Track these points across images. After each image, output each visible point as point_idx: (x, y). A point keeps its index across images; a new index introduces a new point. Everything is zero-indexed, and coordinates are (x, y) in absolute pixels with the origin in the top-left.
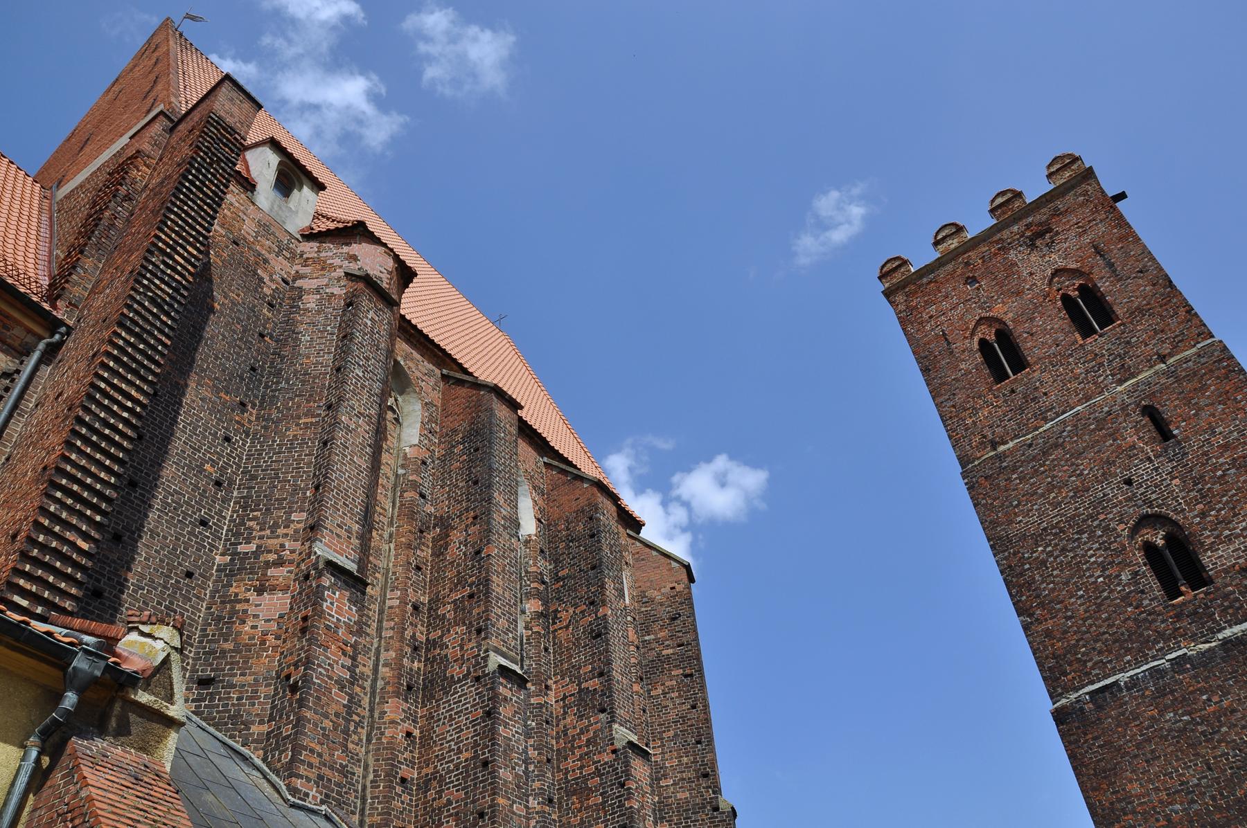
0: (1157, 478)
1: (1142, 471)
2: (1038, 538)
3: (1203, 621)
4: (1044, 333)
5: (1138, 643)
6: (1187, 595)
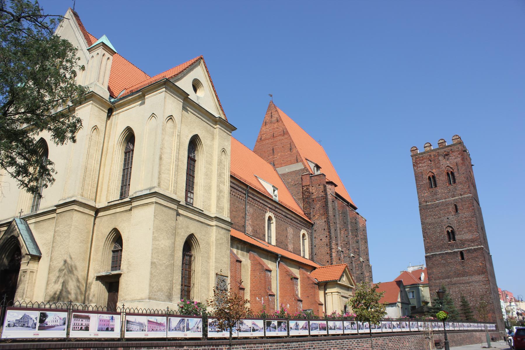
0: (452, 219)
1: (451, 217)
2: (430, 224)
3: (452, 246)
4: (442, 179)
5: (441, 248)
6: (452, 242)
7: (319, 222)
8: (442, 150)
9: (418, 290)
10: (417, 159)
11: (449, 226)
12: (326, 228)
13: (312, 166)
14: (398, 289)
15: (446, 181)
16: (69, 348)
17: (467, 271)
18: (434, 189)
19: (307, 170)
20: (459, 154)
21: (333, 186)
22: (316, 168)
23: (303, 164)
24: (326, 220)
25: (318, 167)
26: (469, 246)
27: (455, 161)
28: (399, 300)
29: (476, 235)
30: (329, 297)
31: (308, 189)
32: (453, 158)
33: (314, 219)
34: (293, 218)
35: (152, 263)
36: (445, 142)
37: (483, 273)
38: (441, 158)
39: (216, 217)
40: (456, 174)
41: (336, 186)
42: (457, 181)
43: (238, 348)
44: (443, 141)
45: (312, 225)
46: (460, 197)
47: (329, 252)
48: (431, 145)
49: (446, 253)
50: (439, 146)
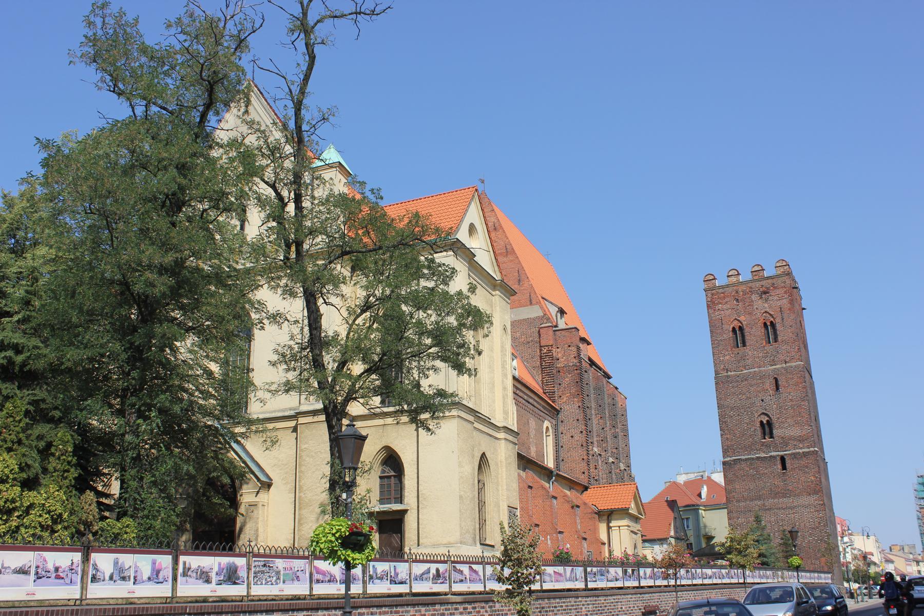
0: (772, 404)
3: (768, 446)
4: (755, 334)
5: (749, 448)
6: (768, 439)
7: (569, 407)
8: (758, 284)
9: (697, 515)
10: (715, 296)
11: (763, 413)
12: (581, 417)
13: (553, 310)
14: (671, 515)
15: (758, 331)
16: (232, 613)
17: (790, 488)
18: (741, 350)
19: (548, 319)
20: (785, 292)
21: (585, 345)
22: (559, 314)
23: (542, 308)
24: (580, 404)
25: (562, 312)
26: (795, 447)
27: (779, 303)
28: (672, 533)
29: (806, 430)
30: (615, 534)
31: (550, 351)
32: (776, 298)
33: (560, 401)
34: (535, 404)
35: (461, 497)
36: (763, 270)
37: (816, 492)
38: (754, 297)
39: (505, 427)
40: (778, 326)
41: (589, 343)
42: (779, 338)
43: (387, 613)
44: (759, 268)
45: (558, 412)
46: (784, 365)
47: (585, 457)
48: (739, 274)
49: (758, 458)
50: (753, 276)
